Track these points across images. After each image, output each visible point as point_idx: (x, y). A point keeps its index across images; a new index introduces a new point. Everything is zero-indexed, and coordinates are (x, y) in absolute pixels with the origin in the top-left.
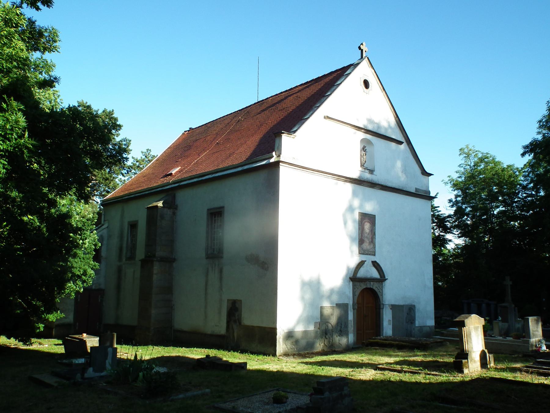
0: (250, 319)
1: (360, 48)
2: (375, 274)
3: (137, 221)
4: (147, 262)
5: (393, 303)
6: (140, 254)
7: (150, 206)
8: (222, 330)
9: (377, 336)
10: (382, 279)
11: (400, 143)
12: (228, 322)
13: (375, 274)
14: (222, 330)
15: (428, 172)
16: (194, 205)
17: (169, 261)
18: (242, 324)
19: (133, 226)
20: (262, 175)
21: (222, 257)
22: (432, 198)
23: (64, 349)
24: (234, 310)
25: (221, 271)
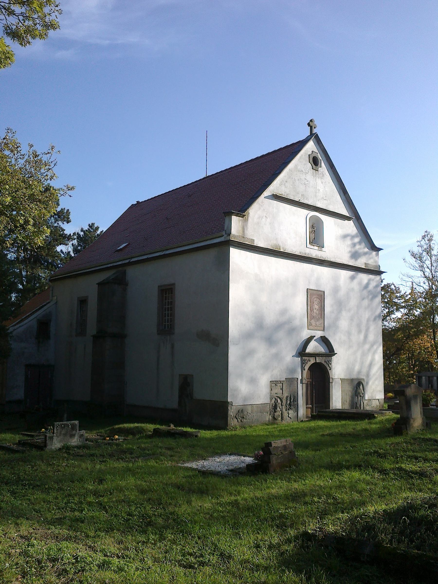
0: (201, 393)
1: (309, 124)
2: (321, 349)
3: (87, 297)
4: (99, 337)
5: (341, 378)
6: (92, 328)
7: (119, 248)
8: (174, 405)
9: (326, 408)
10: (331, 352)
11: (348, 218)
12: (180, 397)
13: (321, 349)
14: (174, 405)
15: (378, 247)
16: (145, 281)
17: (120, 337)
18: (194, 398)
19: (83, 302)
20: (213, 252)
21: (173, 334)
22: (382, 273)
23: (238, 295)
24: (186, 384)
25: (173, 347)
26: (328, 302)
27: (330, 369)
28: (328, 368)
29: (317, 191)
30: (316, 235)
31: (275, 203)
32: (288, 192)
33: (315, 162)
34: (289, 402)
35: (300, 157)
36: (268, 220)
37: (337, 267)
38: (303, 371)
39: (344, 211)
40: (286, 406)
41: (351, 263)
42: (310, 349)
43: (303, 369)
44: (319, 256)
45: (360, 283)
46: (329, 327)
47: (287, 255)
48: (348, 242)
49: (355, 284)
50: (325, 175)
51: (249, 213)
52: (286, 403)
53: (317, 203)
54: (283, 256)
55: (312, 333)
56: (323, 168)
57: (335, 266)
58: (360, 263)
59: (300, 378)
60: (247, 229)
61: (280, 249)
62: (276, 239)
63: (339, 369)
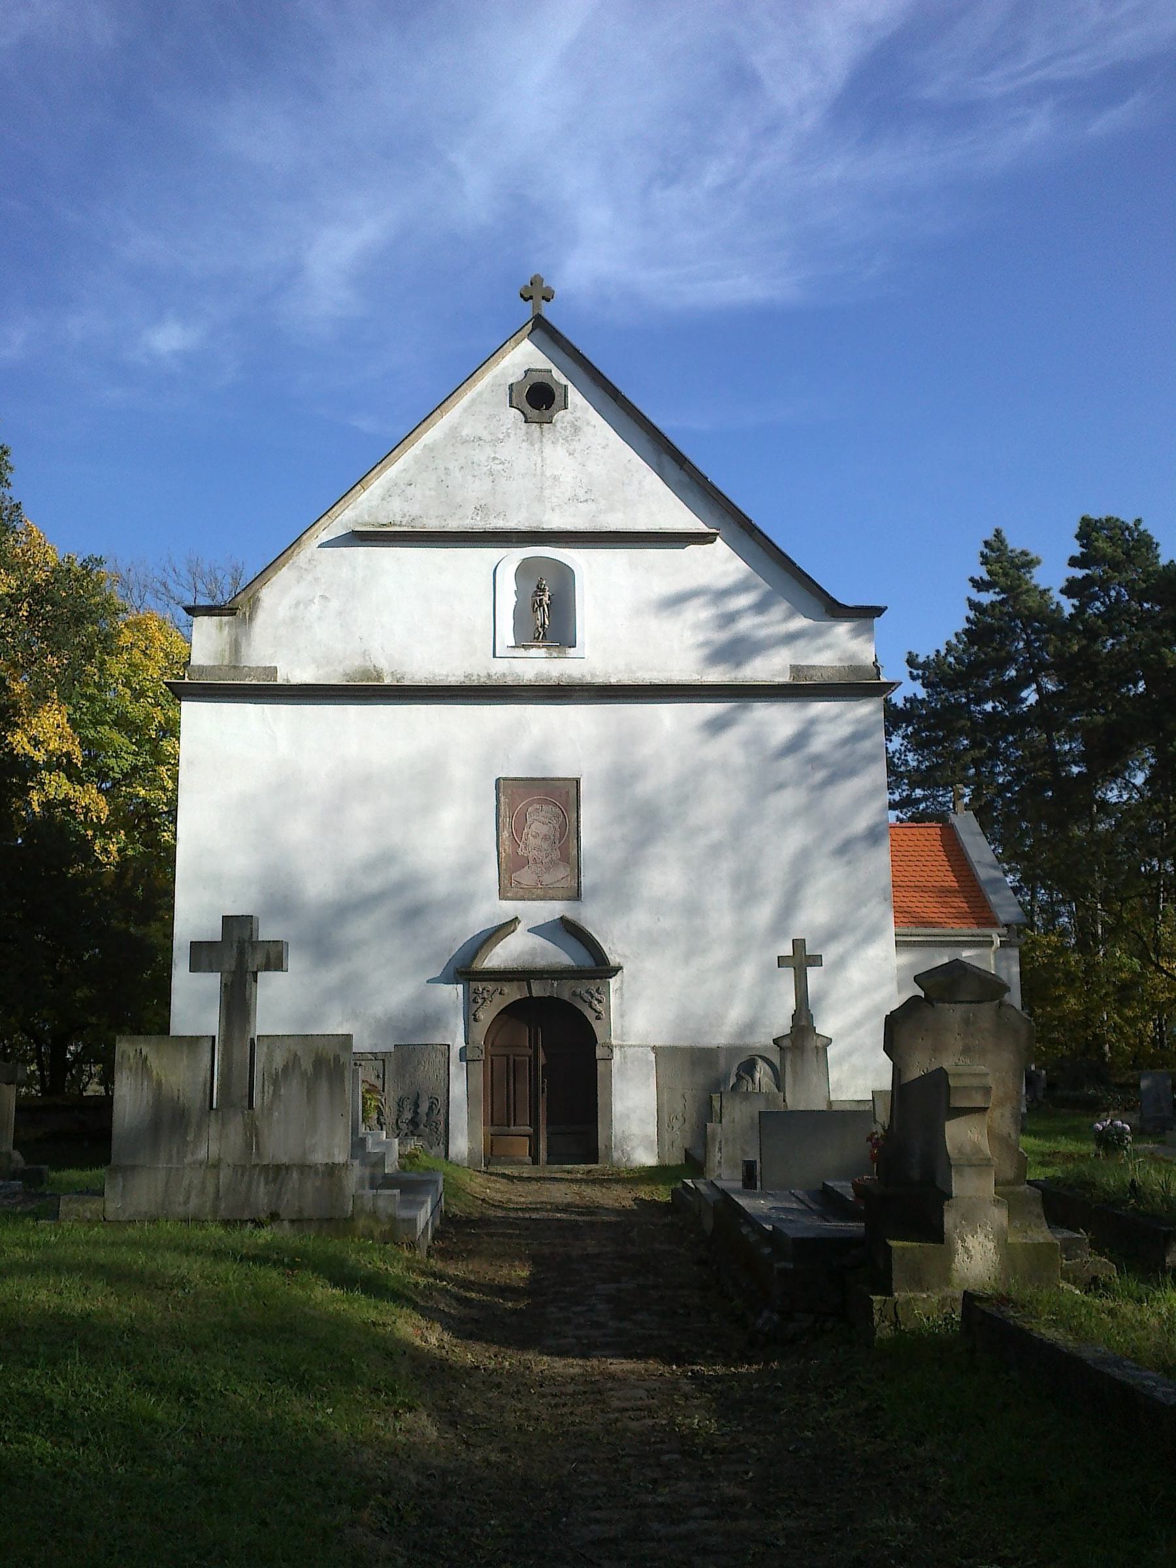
2: (558, 956)
5: (658, 1044)
15: (850, 605)
26: (591, 815)
27: (598, 1018)
28: (590, 1015)
29: (549, 483)
30: (548, 613)
31: (362, 554)
32: (414, 510)
33: (539, 399)
34: (408, 1115)
35: (473, 401)
36: (335, 604)
37: (719, 696)
38: (473, 1023)
39: (685, 519)
40: (398, 1128)
41: (715, 676)
42: (499, 956)
43: (471, 1018)
44: (483, 673)
45: (755, 742)
46: (595, 889)
47: (397, 690)
48: (700, 612)
49: (729, 744)
50: (586, 429)
51: (258, 599)
52: (399, 1117)
53: (546, 518)
54: (610, 697)
55: (510, 908)
56: (578, 405)
57: (689, 696)
58: (769, 668)
59: (460, 1042)
60: (249, 645)
61: (379, 677)
62: (365, 653)
63: (640, 1017)
